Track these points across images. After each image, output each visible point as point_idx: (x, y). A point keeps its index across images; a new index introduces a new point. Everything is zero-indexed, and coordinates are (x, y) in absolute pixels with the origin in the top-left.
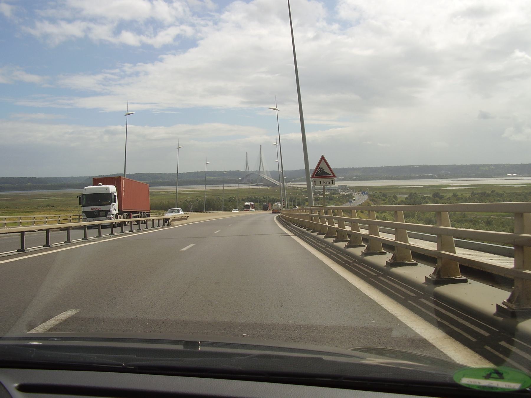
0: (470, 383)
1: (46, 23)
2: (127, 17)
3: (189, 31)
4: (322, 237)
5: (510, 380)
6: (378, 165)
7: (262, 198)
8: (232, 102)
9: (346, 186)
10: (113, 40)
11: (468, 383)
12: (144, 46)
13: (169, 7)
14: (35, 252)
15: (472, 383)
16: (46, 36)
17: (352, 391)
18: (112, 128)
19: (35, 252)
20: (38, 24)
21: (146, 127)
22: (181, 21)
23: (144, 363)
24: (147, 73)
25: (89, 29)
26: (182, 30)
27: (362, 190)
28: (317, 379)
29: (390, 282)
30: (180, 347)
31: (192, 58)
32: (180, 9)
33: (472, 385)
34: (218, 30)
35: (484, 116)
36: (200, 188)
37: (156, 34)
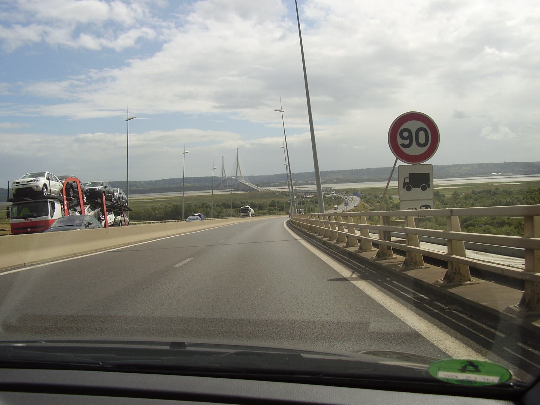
0: (447, 377)
2: (84, 19)
3: (150, 33)
7: (239, 203)
8: (204, 106)
9: (331, 188)
10: (71, 44)
11: (444, 377)
12: (105, 50)
13: (127, 8)
15: (450, 377)
17: (328, 387)
18: (82, 136)
21: (117, 134)
22: (142, 24)
25: (46, 33)
27: (355, 192)
28: (295, 376)
30: (167, 348)
31: (160, 62)
32: (139, 10)
33: (450, 380)
34: (185, 32)
35: (460, 115)
36: (179, 194)
37: (116, 37)
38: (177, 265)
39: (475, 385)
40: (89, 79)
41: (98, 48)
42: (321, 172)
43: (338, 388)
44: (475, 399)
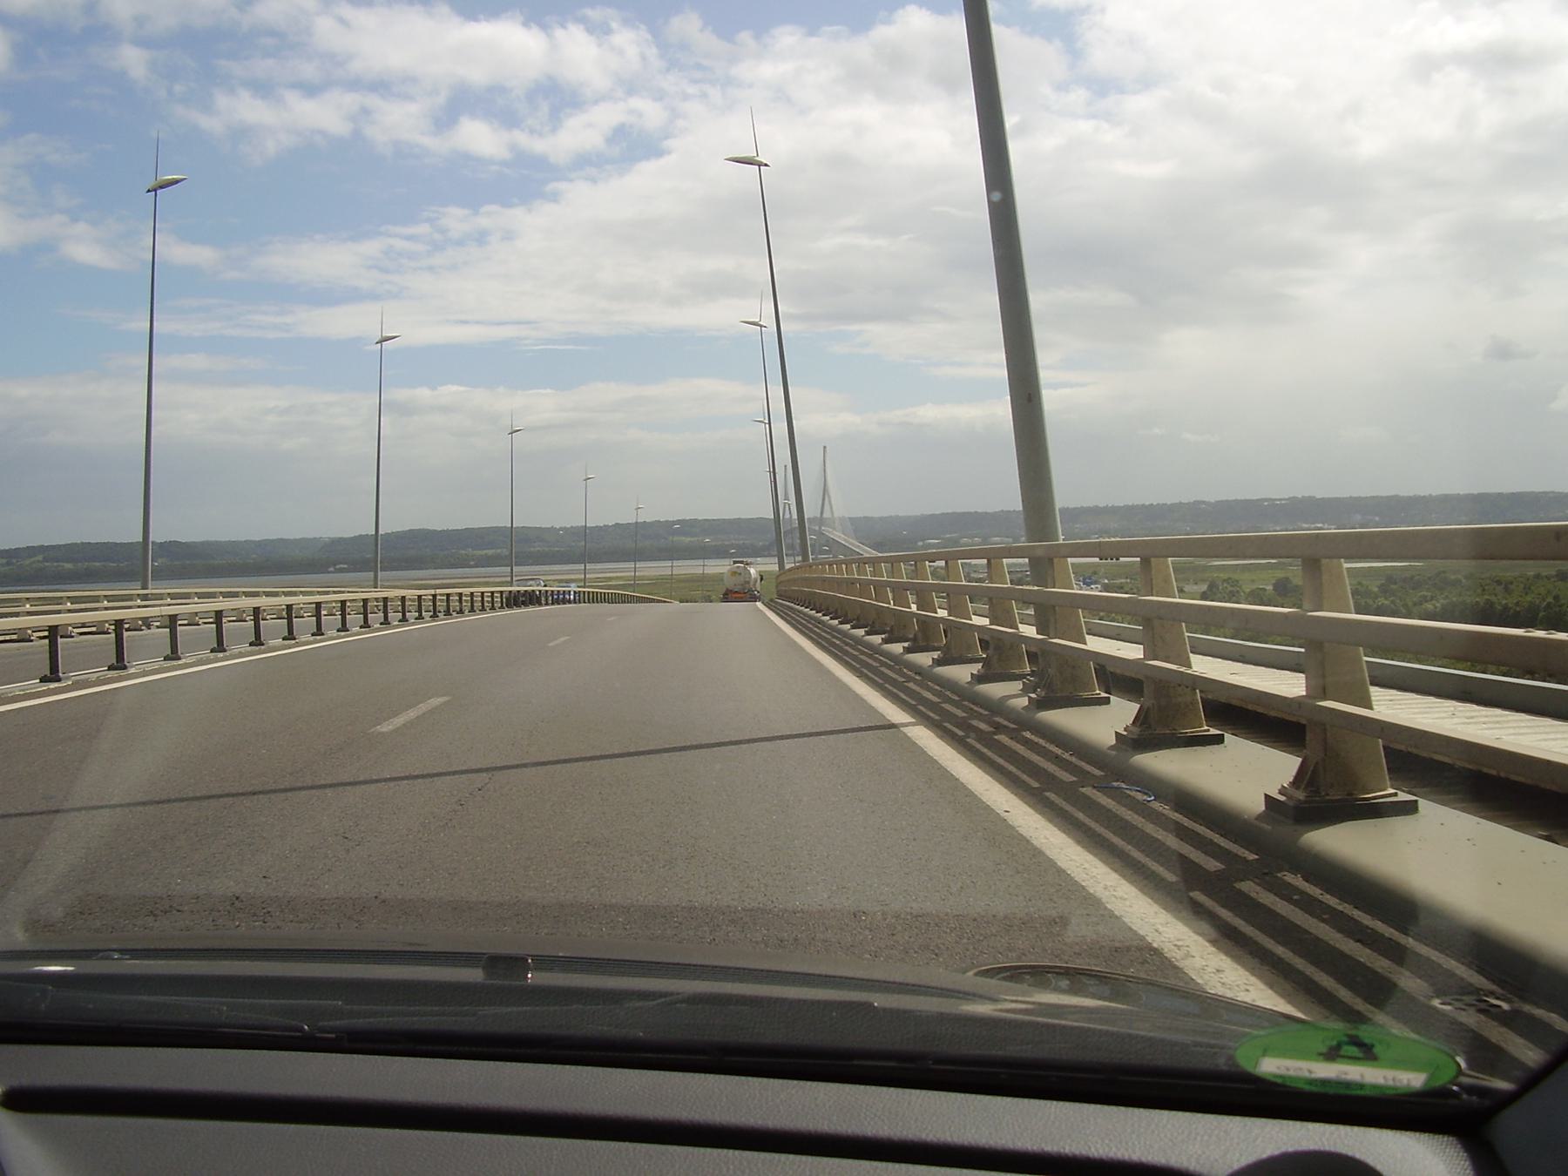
0: (1283, 1072)
1: (245, 95)
2: (477, 76)
3: (651, 113)
4: (877, 639)
5: (1397, 1064)
6: (1169, 499)
10: (430, 142)
13: (600, 45)
14: (87, 683)
15: (1292, 1073)
16: (242, 133)
19: (87, 683)
20: (222, 101)
21: (501, 389)
22: (631, 86)
23: (360, 1023)
24: (509, 236)
25: (366, 112)
26: (631, 112)
29: (1035, 758)
30: (474, 975)
32: (632, 52)
35: (1502, 351)
38: (385, 728)
39: (1361, 1093)
40: (437, 236)
41: (503, 153)
42: (1064, 511)
43: (980, 1097)
44: (1356, 1129)
